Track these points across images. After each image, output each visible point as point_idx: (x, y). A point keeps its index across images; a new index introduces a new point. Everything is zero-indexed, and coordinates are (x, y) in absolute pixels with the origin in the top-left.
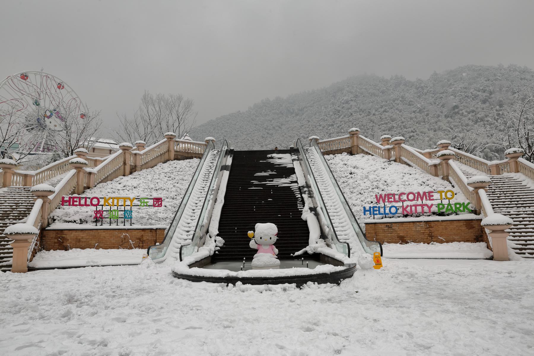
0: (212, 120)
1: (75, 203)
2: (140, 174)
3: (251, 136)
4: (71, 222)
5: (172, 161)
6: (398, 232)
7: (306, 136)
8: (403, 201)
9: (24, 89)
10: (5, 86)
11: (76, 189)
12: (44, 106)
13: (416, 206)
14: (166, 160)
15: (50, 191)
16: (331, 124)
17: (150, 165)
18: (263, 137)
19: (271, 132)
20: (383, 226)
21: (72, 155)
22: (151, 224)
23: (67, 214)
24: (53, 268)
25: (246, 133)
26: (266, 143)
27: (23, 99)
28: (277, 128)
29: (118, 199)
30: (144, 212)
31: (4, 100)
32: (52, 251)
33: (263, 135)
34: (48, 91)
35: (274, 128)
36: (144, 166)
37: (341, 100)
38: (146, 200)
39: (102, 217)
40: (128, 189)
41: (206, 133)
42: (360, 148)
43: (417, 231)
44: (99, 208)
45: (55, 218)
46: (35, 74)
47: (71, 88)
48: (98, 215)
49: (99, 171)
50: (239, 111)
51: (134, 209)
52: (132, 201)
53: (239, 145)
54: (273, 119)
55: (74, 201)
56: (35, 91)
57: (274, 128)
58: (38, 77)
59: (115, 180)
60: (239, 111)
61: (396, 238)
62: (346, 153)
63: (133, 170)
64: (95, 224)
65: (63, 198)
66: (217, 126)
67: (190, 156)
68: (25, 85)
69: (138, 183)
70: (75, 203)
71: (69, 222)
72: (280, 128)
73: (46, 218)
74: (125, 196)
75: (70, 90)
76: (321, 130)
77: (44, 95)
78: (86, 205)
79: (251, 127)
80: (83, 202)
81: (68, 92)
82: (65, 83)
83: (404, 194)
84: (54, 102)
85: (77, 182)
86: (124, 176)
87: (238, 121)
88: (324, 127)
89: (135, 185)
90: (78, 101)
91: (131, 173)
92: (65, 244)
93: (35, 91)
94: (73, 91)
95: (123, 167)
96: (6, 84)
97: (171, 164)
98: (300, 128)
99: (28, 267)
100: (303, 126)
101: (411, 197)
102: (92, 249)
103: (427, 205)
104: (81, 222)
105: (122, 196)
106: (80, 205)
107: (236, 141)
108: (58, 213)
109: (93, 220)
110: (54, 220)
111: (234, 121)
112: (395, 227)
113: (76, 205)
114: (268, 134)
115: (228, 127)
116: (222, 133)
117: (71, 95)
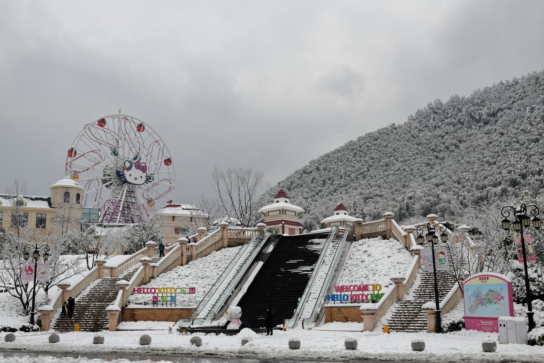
0: (351, 141)
1: (141, 292)
2: (194, 263)
3: (410, 164)
4: (139, 304)
5: (225, 248)
6: (344, 314)
7: (492, 161)
9: (102, 138)
10: (83, 138)
11: (144, 279)
12: (123, 155)
13: (359, 295)
14: (220, 247)
15: (127, 285)
16: (535, 137)
17: (204, 254)
18: (428, 165)
19: (441, 155)
21: (144, 247)
22: (189, 305)
23: (137, 299)
24: (127, 330)
25: (402, 159)
26: (431, 173)
27: (101, 150)
28: (452, 148)
29: (167, 288)
32: (128, 322)
33: (429, 162)
34: (127, 136)
35: (447, 148)
36: (199, 255)
38: (185, 289)
40: (181, 278)
41: (342, 161)
42: (392, 232)
43: (355, 313)
44: (156, 295)
45: (130, 301)
47: (152, 129)
48: (155, 299)
49: (160, 264)
50: (394, 124)
53: (389, 180)
54: (447, 133)
55: (140, 291)
56: (113, 139)
57: (447, 148)
58: (116, 120)
59: (173, 269)
60: (394, 124)
61: (343, 318)
63: (190, 259)
64: (153, 305)
66: (360, 151)
67: (242, 242)
68: (102, 133)
69: (190, 272)
70: (141, 292)
71: (138, 304)
72: (457, 146)
73: (125, 301)
74: (171, 287)
76: (517, 150)
77: (123, 141)
78: (148, 293)
79: (410, 149)
80: (146, 290)
82: (145, 124)
83: (352, 286)
84: (133, 149)
85: (145, 275)
86: (182, 265)
87: (390, 141)
88: (522, 145)
89: (187, 274)
90: (162, 144)
91: (187, 263)
92: (135, 318)
93: (113, 139)
94: (155, 132)
95: (180, 258)
97: (223, 252)
98: (486, 146)
99: (116, 329)
100: (491, 143)
101: (356, 288)
102: (151, 321)
103: (364, 294)
104: (145, 304)
105: (169, 287)
106: (144, 293)
107: (386, 173)
108: (132, 298)
109: (152, 303)
110: (130, 303)
111: (385, 140)
112: (343, 310)
113: (142, 293)
114: (437, 157)
115: (375, 151)
116: (366, 162)
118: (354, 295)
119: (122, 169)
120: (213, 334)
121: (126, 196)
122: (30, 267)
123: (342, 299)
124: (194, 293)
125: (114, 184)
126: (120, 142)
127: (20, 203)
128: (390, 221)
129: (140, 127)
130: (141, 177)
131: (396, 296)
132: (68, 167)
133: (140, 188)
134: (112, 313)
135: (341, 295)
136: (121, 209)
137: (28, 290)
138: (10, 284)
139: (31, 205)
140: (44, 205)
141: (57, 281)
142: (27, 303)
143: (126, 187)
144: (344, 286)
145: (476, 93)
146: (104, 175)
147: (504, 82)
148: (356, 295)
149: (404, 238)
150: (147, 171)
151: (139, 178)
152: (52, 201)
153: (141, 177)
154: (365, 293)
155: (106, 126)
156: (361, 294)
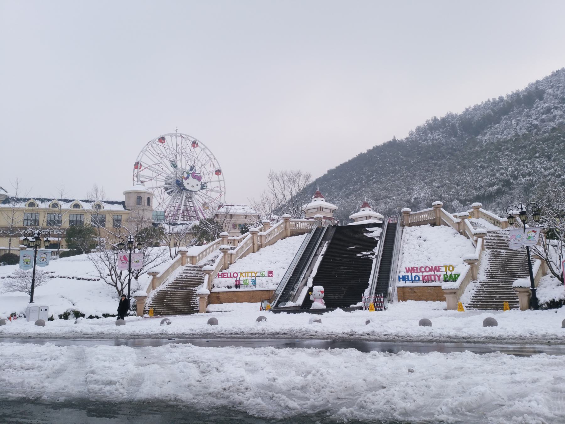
8: (423, 272)
10: (146, 153)
13: (431, 275)
17: (272, 243)
20: (408, 289)
23: (220, 283)
27: (163, 162)
30: (264, 279)
31: (147, 166)
34: (183, 151)
37: (539, 109)
38: (264, 273)
39: (239, 284)
44: (238, 279)
46: (171, 136)
49: (237, 252)
51: (257, 278)
52: (256, 274)
55: (224, 275)
56: (172, 154)
62: (430, 225)
63: (260, 246)
65: (218, 274)
67: (302, 231)
75: (203, 147)
78: (231, 277)
80: (229, 275)
81: (202, 149)
82: (198, 141)
83: (423, 267)
84: (189, 162)
86: (254, 252)
91: (258, 250)
93: (172, 154)
94: (206, 147)
96: (147, 151)
101: (428, 269)
103: (437, 275)
106: (228, 277)
117: (205, 152)
118: (426, 276)
119: (181, 179)
120: (285, 313)
121: (185, 201)
122: (124, 256)
123: (413, 280)
124: (272, 276)
125: (175, 191)
126: (178, 156)
127: (99, 206)
128: (440, 210)
129: (194, 144)
130: (197, 185)
131: (472, 276)
132: (135, 178)
133: (196, 194)
134: (202, 296)
135: (411, 276)
136: (181, 212)
137: (123, 277)
138: (554, 246)
139: (107, 207)
140: (120, 208)
141: (146, 269)
142: (122, 290)
143: (185, 194)
144: (414, 268)
145: (467, 110)
146: (166, 184)
147: (491, 100)
148: (427, 276)
149: (457, 225)
150: (202, 181)
151: (195, 186)
152: (126, 204)
153: (197, 185)
154: (436, 273)
155: (165, 143)
156: (433, 275)
